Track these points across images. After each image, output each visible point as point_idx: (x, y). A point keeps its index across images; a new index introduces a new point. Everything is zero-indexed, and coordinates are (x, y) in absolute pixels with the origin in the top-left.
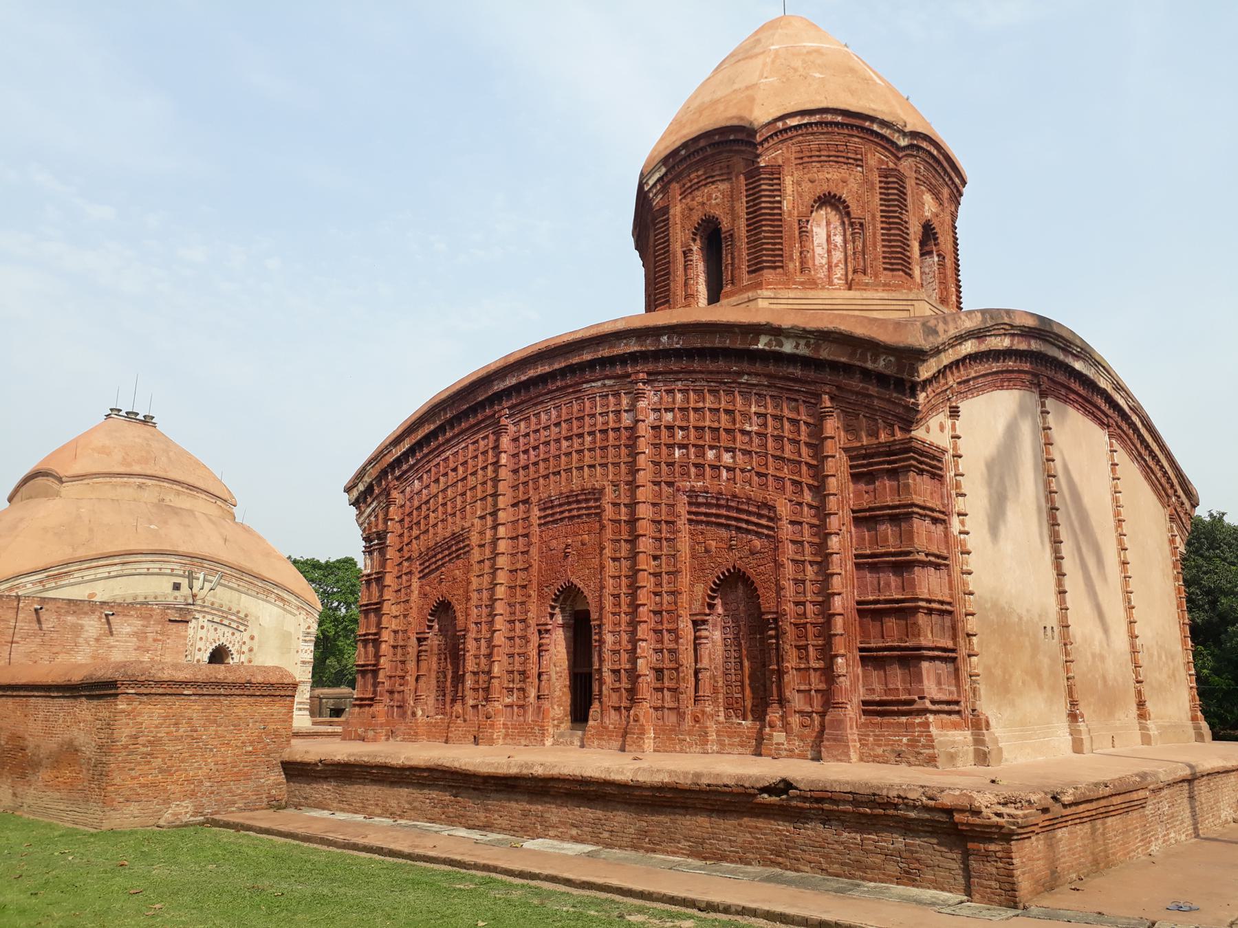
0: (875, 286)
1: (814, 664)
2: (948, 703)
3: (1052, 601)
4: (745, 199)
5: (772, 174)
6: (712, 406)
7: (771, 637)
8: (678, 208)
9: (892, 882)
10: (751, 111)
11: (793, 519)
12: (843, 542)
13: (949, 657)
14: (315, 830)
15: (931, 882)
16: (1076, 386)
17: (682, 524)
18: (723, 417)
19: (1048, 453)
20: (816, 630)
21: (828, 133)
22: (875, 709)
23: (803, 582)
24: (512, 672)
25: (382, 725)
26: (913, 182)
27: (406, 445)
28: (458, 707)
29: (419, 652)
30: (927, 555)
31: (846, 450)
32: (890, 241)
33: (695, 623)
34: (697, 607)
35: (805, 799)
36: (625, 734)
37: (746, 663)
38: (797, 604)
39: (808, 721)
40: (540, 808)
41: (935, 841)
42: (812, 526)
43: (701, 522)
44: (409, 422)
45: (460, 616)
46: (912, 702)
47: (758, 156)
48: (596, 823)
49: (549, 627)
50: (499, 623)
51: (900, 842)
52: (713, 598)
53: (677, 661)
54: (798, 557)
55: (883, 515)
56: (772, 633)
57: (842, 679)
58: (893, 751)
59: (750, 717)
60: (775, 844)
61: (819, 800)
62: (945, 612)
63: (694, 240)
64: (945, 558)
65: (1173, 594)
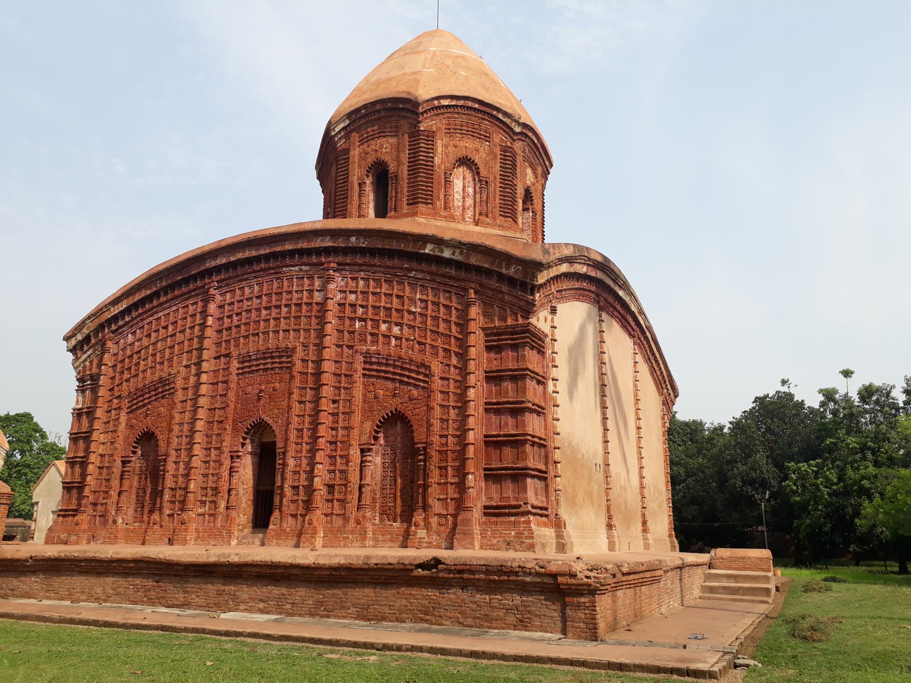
0: (494, 226)
1: (450, 480)
2: (541, 508)
3: (600, 446)
4: (407, 152)
5: (428, 136)
6: (387, 292)
7: (420, 461)
8: (357, 151)
9: (510, 629)
10: (417, 89)
11: (443, 376)
12: (478, 393)
13: (542, 476)
14: (27, 611)
15: (538, 627)
16: (618, 307)
17: (358, 377)
18: (395, 300)
19: (602, 348)
20: (454, 456)
21: (468, 114)
22: (493, 512)
23: (447, 421)
24: (206, 488)
25: (84, 531)
26: (521, 158)
27: (123, 305)
28: (156, 516)
29: (123, 472)
30: (533, 405)
31: (483, 329)
32: (505, 196)
33: (362, 451)
35: (450, 571)
36: (300, 535)
37: (399, 481)
38: (441, 436)
39: (443, 521)
40: (233, 588)
41: (543, 598)
42: (456, 381)
43: (373, 376)
44: (128, 287)
45: (162, 445)
46: (519, 506)
47: (420, 122)
48: (280, 598)
49: (241, 454)
50: (197, 449)
51: (517, 599)
52: (378, 432)
53: (346, 479)
54: (444, 403)
55: (506, 376)
56: (421, 457)
57: (471, 490)
58: (504, 541)
59: (399, 520)
60: (424, 606)
61: (461, 572)
62: (541, 444)
63: (368, 176)
64: (543, 409)
65: (662, 452)
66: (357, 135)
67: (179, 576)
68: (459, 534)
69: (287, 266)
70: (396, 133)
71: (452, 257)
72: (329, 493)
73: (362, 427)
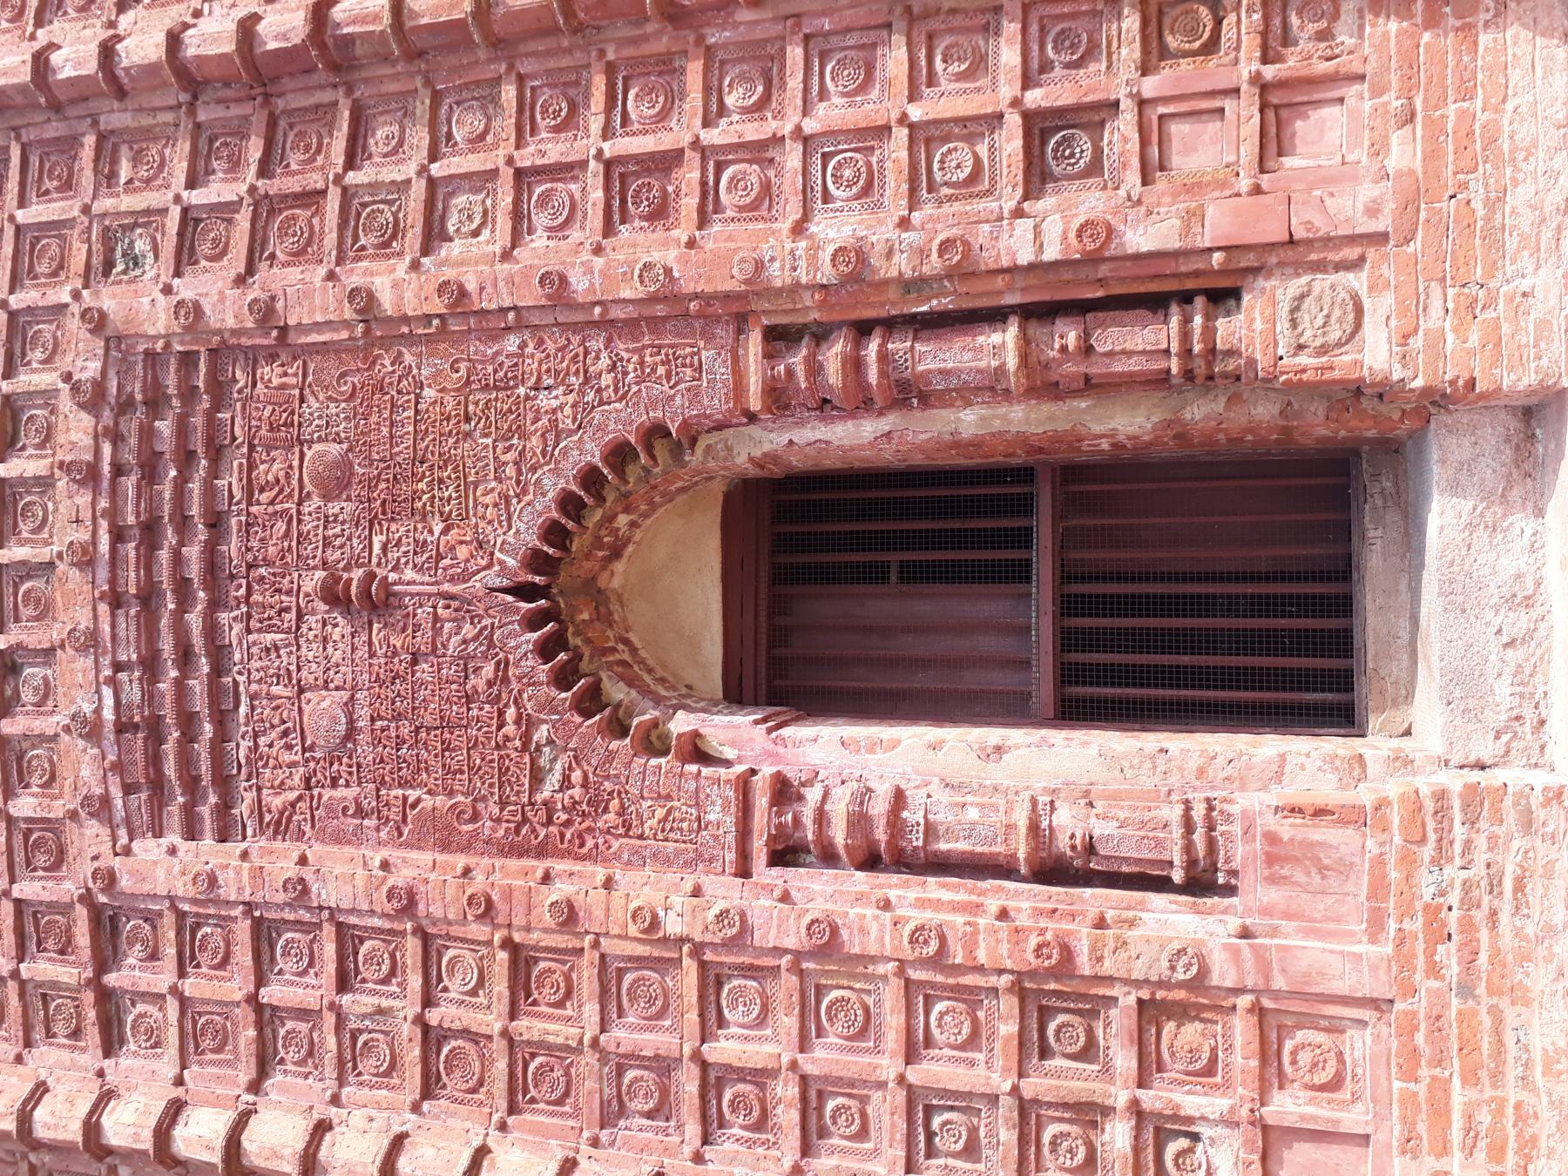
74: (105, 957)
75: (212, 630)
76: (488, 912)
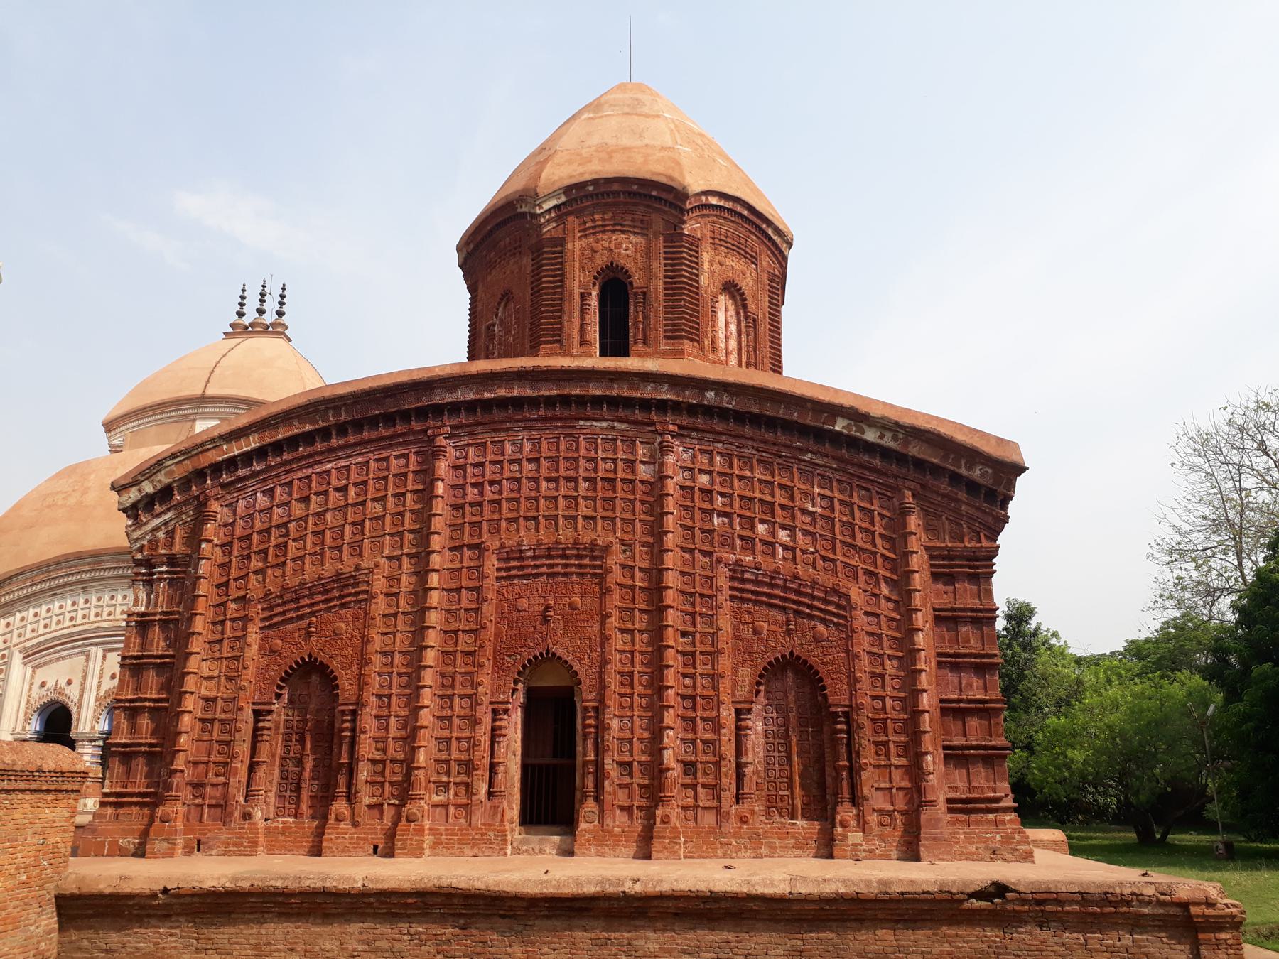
1: (895, 761)
4: (662, 262)
11: (869, 609)
27: (253, 443)
31: (927, 548)
34: (742, 693)
35: (1024, 901)
39: (887, 819)
40: (627, 935)
42: (890, 619)
43: (749, 600)
45: (347, 688)
47: (684, 222)
50: (427, 697)
58: (987, 848)
61: (1039, 902)
66: (577, 221)
67: (514, 917)
68: (927, 839)
69: (587, 419)
70: (642, 228)
71: (879, 441)
72: (686, 774)
73: (737, 679)
74: (470, 547)
75: (542, 574)
76: (481, 647)
